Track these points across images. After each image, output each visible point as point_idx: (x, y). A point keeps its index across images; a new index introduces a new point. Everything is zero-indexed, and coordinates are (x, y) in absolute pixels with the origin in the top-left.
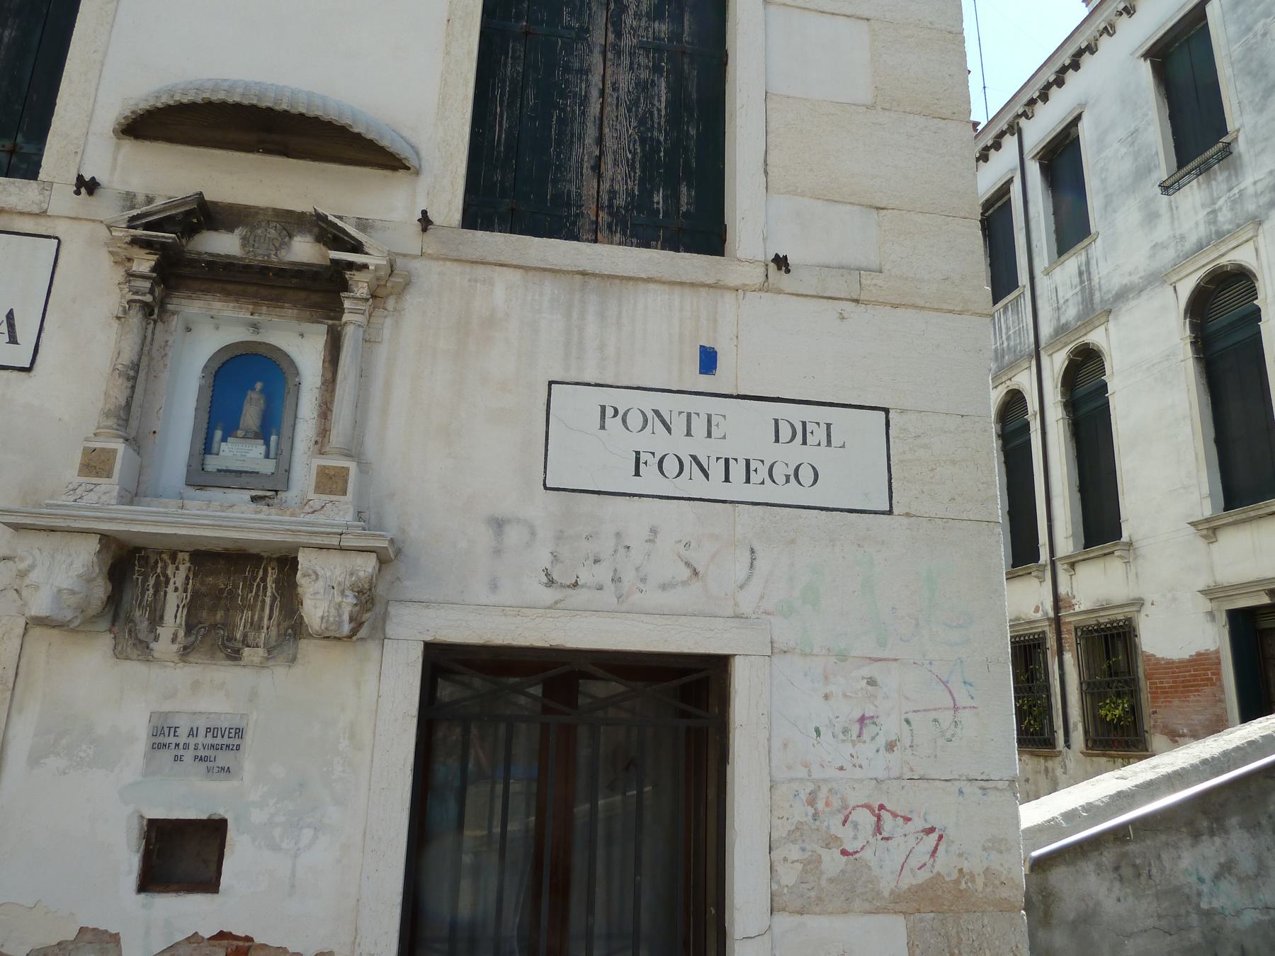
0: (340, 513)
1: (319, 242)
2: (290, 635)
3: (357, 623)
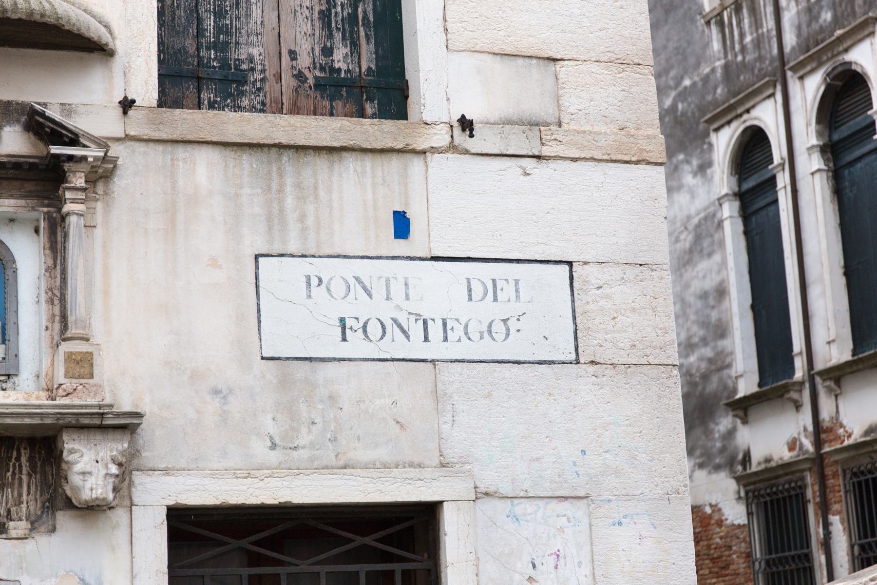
1: (28, 131)
2: (48, 507)
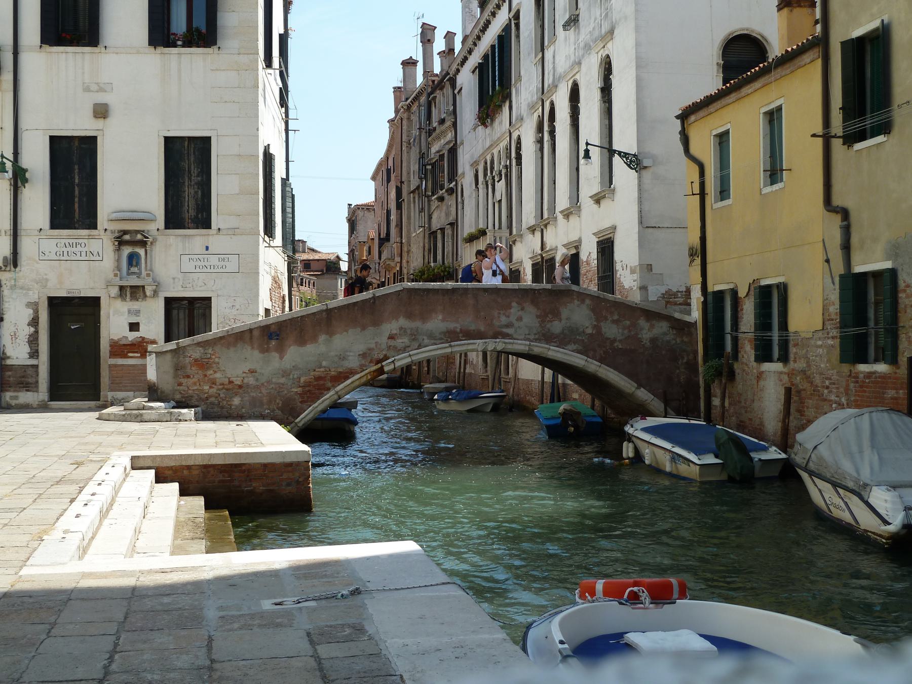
0: (150, 280)
1: (111, 346)
3: (154, 295)
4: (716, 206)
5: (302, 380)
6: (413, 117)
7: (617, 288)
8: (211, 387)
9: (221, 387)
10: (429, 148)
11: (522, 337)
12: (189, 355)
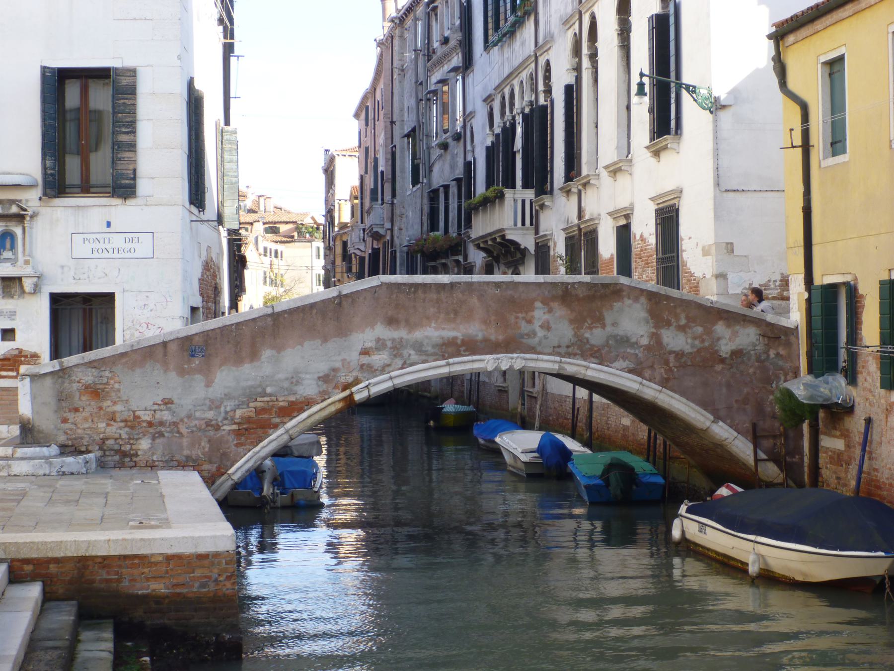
3: (35, 291)
4: (824, 164)
5: (239, 413)
6: (406, 35)
7: (683, 281)
8: (108, 425)
9: (122, 424)
10: (428, 77)
11: (551, 350)
12: (77, 379)
